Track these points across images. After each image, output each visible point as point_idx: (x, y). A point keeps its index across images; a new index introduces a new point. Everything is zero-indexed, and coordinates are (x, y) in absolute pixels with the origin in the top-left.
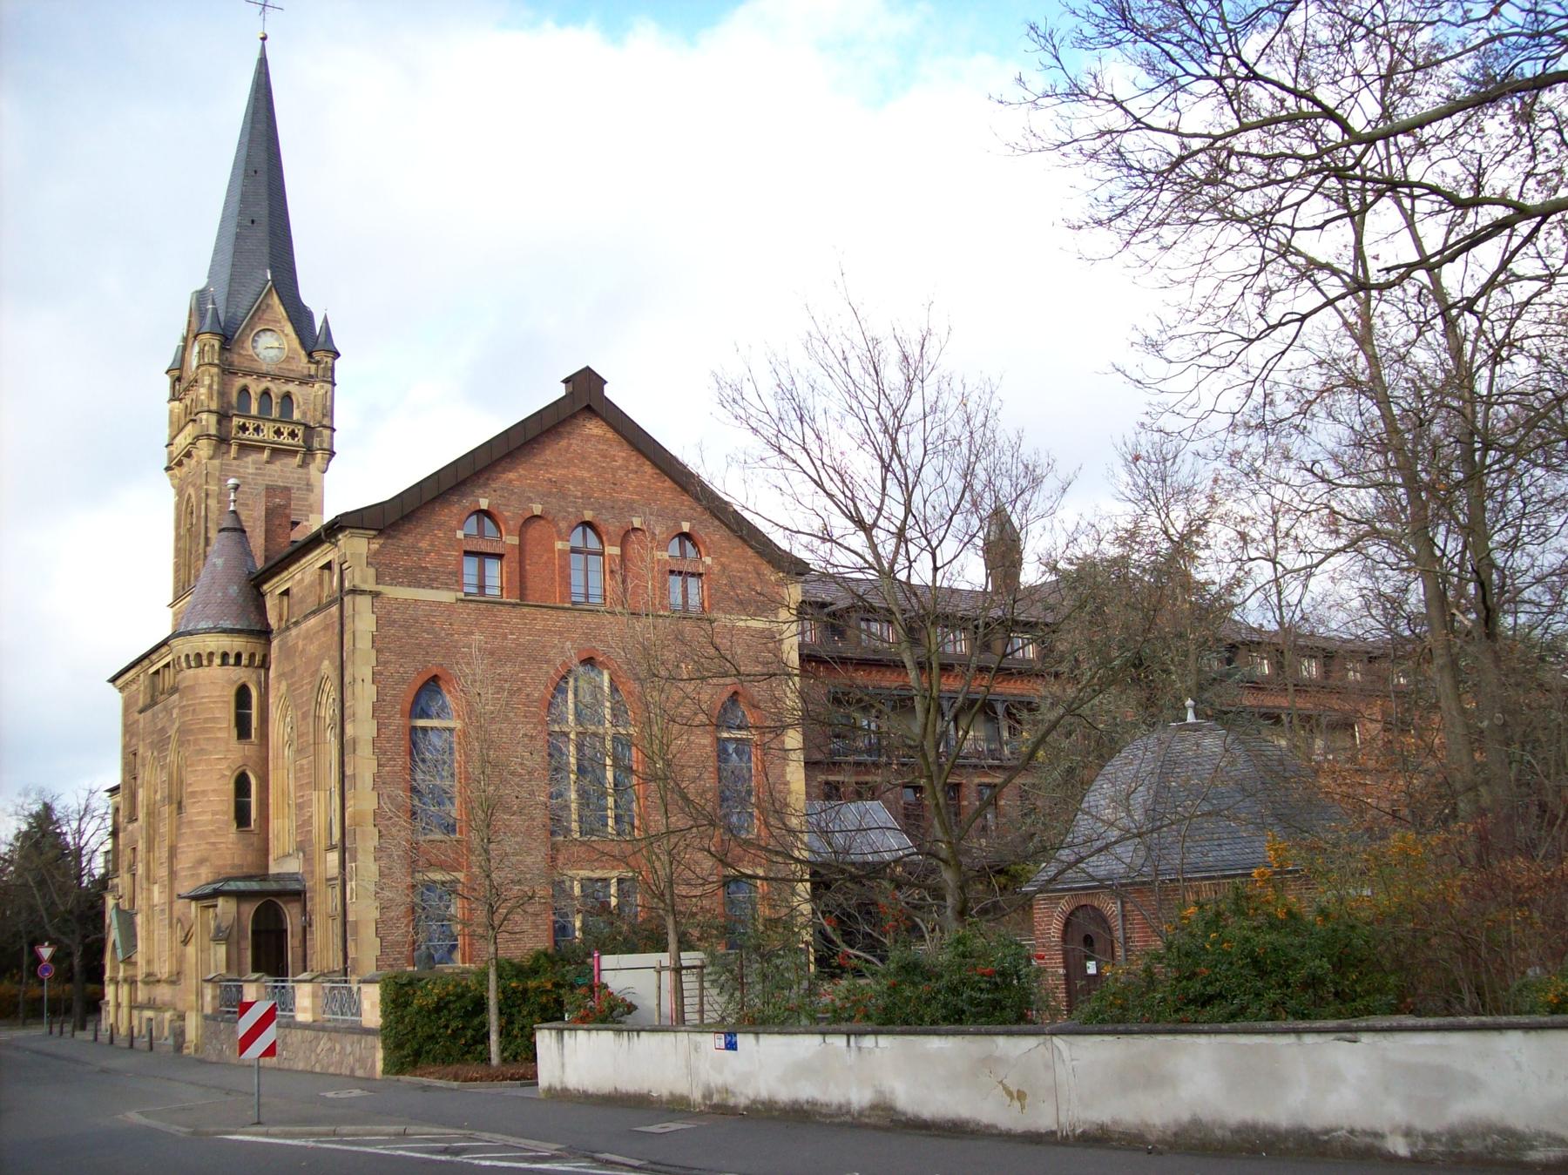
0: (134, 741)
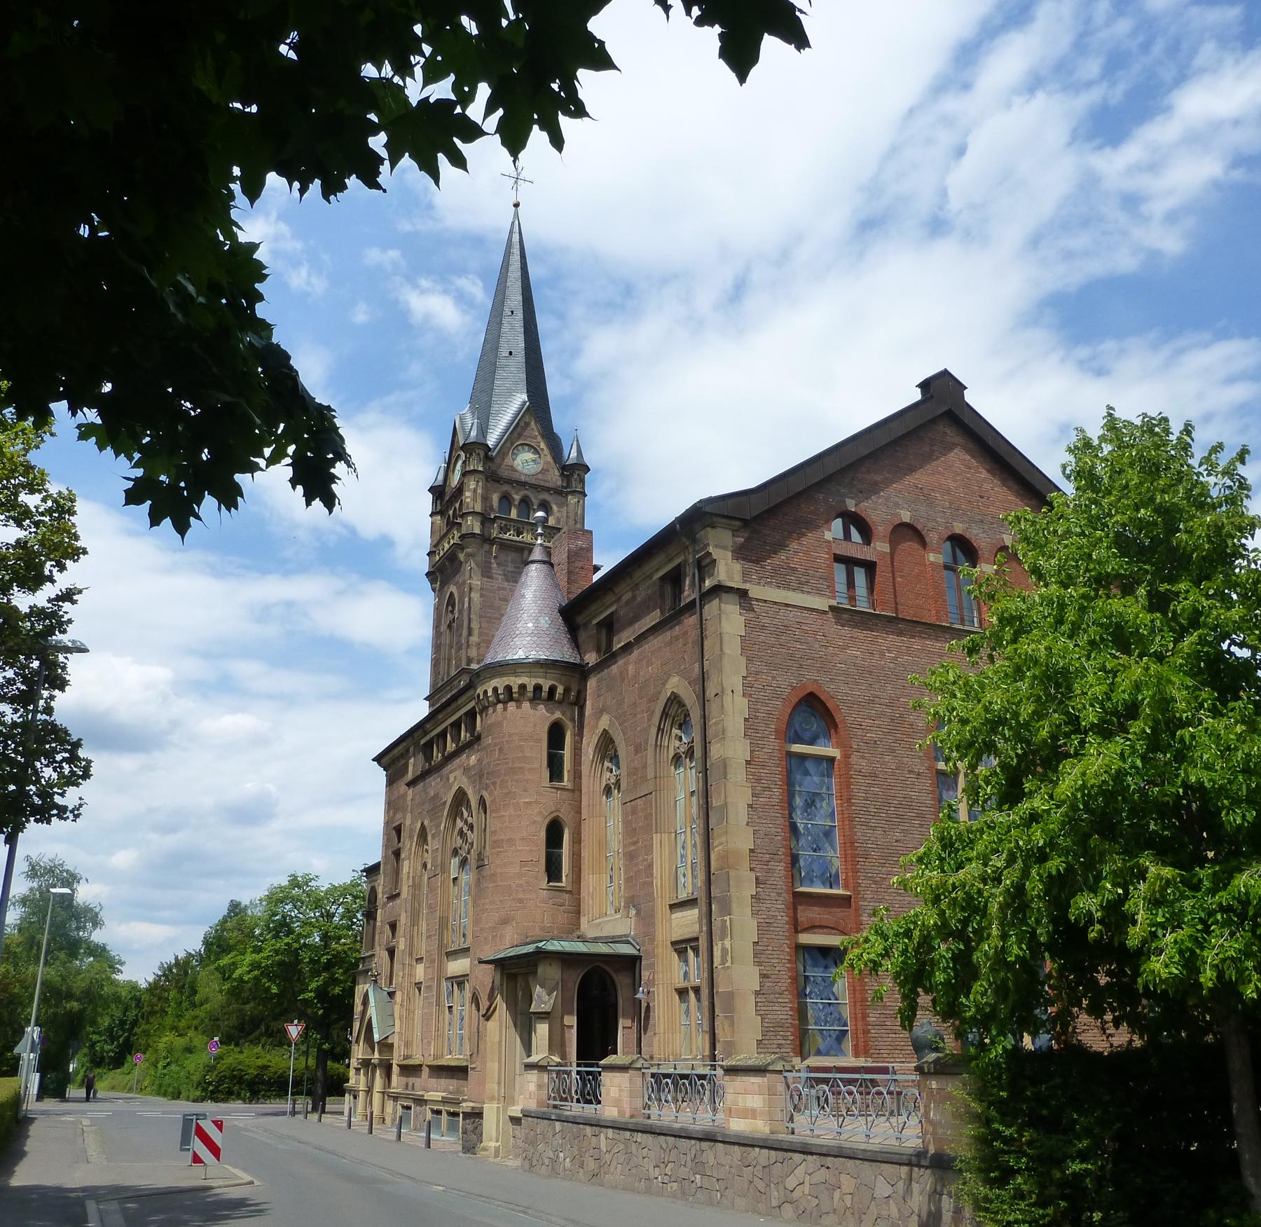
0: (399, 816)
